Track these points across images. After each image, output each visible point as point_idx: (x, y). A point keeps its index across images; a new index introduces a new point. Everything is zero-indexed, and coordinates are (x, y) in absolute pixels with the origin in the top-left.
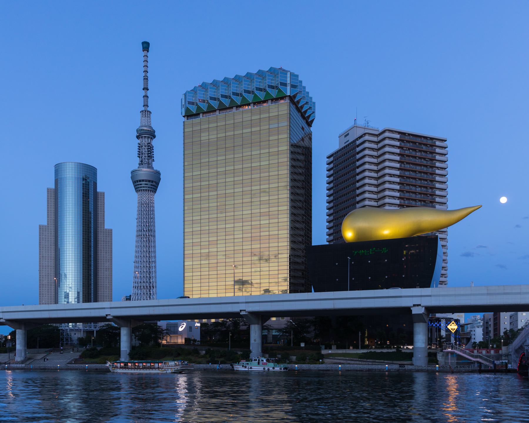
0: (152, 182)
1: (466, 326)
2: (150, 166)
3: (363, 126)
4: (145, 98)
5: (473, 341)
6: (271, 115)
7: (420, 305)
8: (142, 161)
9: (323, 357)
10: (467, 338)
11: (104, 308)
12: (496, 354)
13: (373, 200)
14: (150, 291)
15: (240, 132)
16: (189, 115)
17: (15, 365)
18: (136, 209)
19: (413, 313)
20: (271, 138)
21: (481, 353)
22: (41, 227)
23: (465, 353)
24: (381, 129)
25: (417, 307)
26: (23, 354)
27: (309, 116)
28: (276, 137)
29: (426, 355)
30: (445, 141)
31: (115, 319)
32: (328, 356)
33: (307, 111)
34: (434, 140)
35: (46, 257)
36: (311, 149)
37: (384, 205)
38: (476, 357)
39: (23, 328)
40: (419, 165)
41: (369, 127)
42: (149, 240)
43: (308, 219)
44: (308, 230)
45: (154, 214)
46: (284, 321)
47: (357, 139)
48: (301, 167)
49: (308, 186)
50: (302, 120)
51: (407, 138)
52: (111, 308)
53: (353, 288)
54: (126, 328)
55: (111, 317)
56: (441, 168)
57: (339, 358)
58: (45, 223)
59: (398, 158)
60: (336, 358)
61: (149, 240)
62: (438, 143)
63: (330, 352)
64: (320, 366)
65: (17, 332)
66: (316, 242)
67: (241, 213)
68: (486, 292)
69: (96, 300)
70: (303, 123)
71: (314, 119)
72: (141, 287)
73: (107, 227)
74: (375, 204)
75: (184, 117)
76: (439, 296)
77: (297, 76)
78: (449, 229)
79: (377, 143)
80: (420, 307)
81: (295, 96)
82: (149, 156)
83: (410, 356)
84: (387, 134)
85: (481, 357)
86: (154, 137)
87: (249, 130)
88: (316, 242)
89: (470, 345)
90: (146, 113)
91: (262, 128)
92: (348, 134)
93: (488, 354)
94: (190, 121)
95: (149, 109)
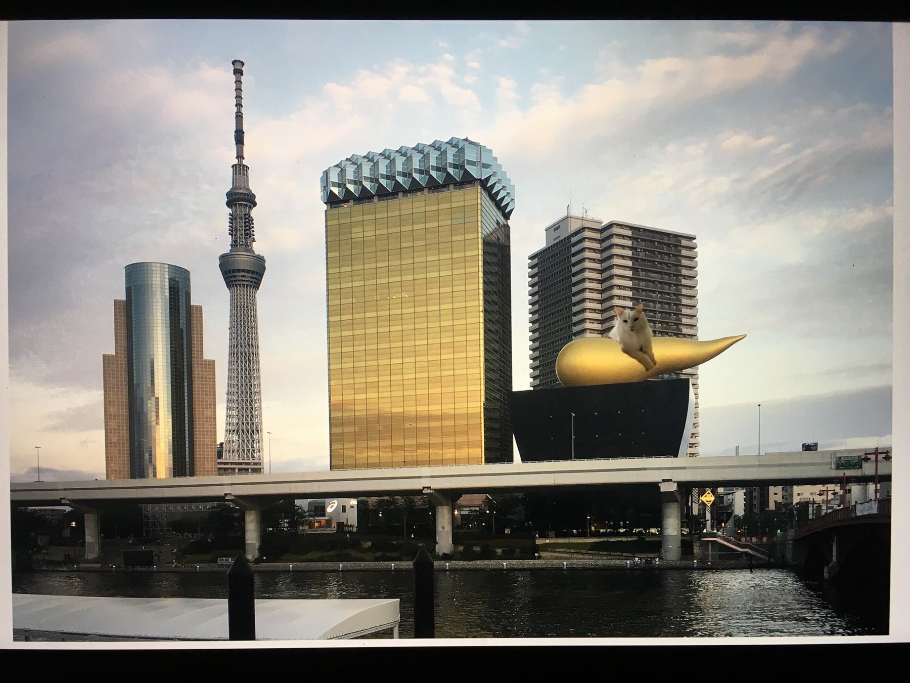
0: (253, 272)
2: (248, 248)
7: (671, 480)
8: (236, 241)
9: (537, 549)
15: (410, 228)
16: (332, 201)
17: (88, 565)
19: (662, 490)
20: (454, 238)
22: (106, 358)
23: (729, 541)
24: (605, 222)
28: (462, 237)
29: (679, 545)
32: (545, 547)
33: (503, 198)
41: (590, 217)
45: (255, 321)
46: (479, 499)
51: (641, 235)
53: (579, 456)
57: (561, 550)
58: (112, 352)
62: (684, 242)
63: (548, 541)
64: (536, 562)
67: (412, 343)
68: (757, 463)
69: (192, 474)
73: (207, 356)
78: (700, 366)
81: (488, 179)
82: (246, 234)
86: (255, 204)
87: (423, 226)
89: (730, 524)
90: (240, 170)
91: (441, 223)
95: (245, 162)
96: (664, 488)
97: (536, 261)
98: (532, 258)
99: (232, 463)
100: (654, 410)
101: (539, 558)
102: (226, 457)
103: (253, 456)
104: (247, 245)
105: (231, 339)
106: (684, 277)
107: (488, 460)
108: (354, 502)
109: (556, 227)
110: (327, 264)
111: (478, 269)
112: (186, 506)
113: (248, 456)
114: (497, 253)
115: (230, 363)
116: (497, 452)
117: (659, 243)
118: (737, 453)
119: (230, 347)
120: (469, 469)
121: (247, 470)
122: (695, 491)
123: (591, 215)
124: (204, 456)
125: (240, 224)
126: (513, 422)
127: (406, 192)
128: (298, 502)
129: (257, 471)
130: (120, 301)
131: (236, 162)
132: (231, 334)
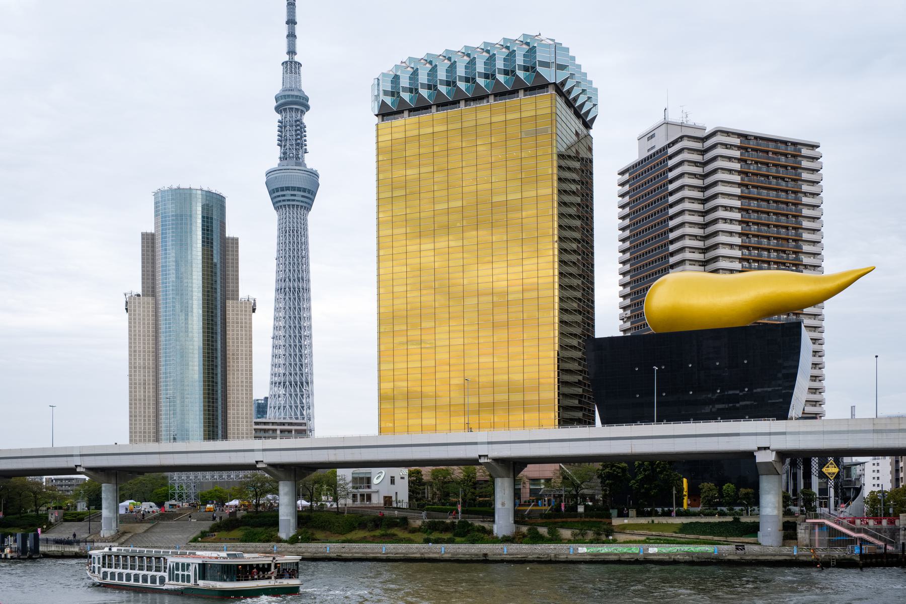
0: (304, 190)
1: (853, 467)
2: (299, 161)
3: (679, 121)
4: (291, 39)
5: (866, 492)
6: (524, 115)
7: (768, 448)
8: (285, 153)
10: (855, 489)
11: (252, 450)
12: (890, 526)
13: (696, 251)
14: (301, 391)
16: (385, 113)
18: (275, 241)
21: (867, 523)
24: (709, 130)
25: (763, 452)
26: (114, 525)
27: (588, 112)
29: (781, 528)
30: (818, 147)
31: (269, 468)
32: (623, 529)
33: (578, 96)
34: (799, 147)
35: (140, 352)
36: (591, 161)
37: (715, 259)
38: (859, 531)
39: (114, 481)
40: (772, 187)
41: (691, 123)
42: (299, 297)
43: (588, 306)
44: (588, 325)
46: (548, 470)
47: (670, 145)
48: (574, 181)
49: (587, 212)
50: (577, 121)
51: (752, 144)
52: (264, 450)
53: (660, 420)
54: (289, 483)
55: (264, 466)
56: (811, 194)
59: (737, 178)
60: (636, 532)
61: (299, 297)
62: (805, 151)
63: (626, 521)
65: (103, 489)
66: (601, 332)
68: (872, 428)
69: (225, 437)
70: (577, 125)
71: (595, 117)
72: (285, 383)
73: (243, 294)
74: (700, 257)
75: (377, 115)
76: (798, 433)
77: (567, 49)
78: (826, 303)
79: (703, 152)
80: (768, 451)
81: (563, 83)
82: (297, 144)
83: (753, 529)
84: (719, 138)
85: (866, 532)
86: (308, 108)
88: (601, 332)
90: (292, 67)
92: (652, 136)
93: (879, 527)
94: (387, 123)
95: (297, 58)
96: (761, 457)
97: (626, 176)
98: (622, 173)
99: (273, 423)
100: (757, 361)
101: (615, 541)
102: (271, 416)
103: (302, 414)
104: (297, 158)
105: (278, 272)
106: (805, 194)
107: (572, 413)
108: (405, 471)
109: (651, 136)
110: (378, 187)
111: (548, 190)
112: (216, 474)
113: (296, 414)
114: (576, 172)
115: (277, 300)
116: (572, 413)
117: (774, 153)
118: (853, 415)
119: (277, 281)
120: (540, 433)
121: (290, 431)
122: (815, 462)
123: (693, 120)
124: (239, 415)
125: (290, 133)
126: (602, 377)
127: (468, 100)
128: (340, 472)
129: (302, 433)
130: (147, 234)
131: (286, 58)
132: (278, 265)
